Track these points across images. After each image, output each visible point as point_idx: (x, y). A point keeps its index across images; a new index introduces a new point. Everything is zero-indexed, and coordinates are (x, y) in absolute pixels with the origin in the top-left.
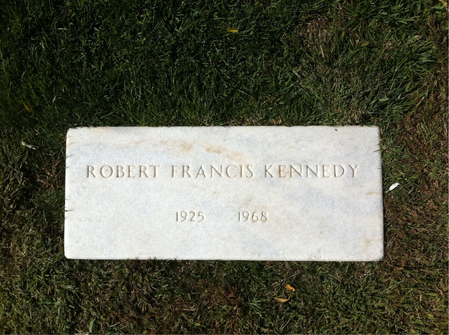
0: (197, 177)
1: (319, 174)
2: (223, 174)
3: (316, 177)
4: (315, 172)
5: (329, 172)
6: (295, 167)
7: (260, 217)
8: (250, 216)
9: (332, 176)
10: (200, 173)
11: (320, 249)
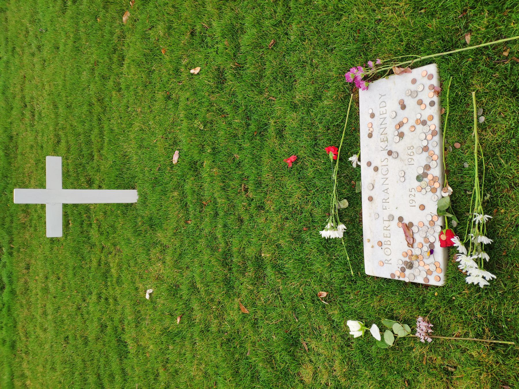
6: (381, 132)
8: (410, 157)
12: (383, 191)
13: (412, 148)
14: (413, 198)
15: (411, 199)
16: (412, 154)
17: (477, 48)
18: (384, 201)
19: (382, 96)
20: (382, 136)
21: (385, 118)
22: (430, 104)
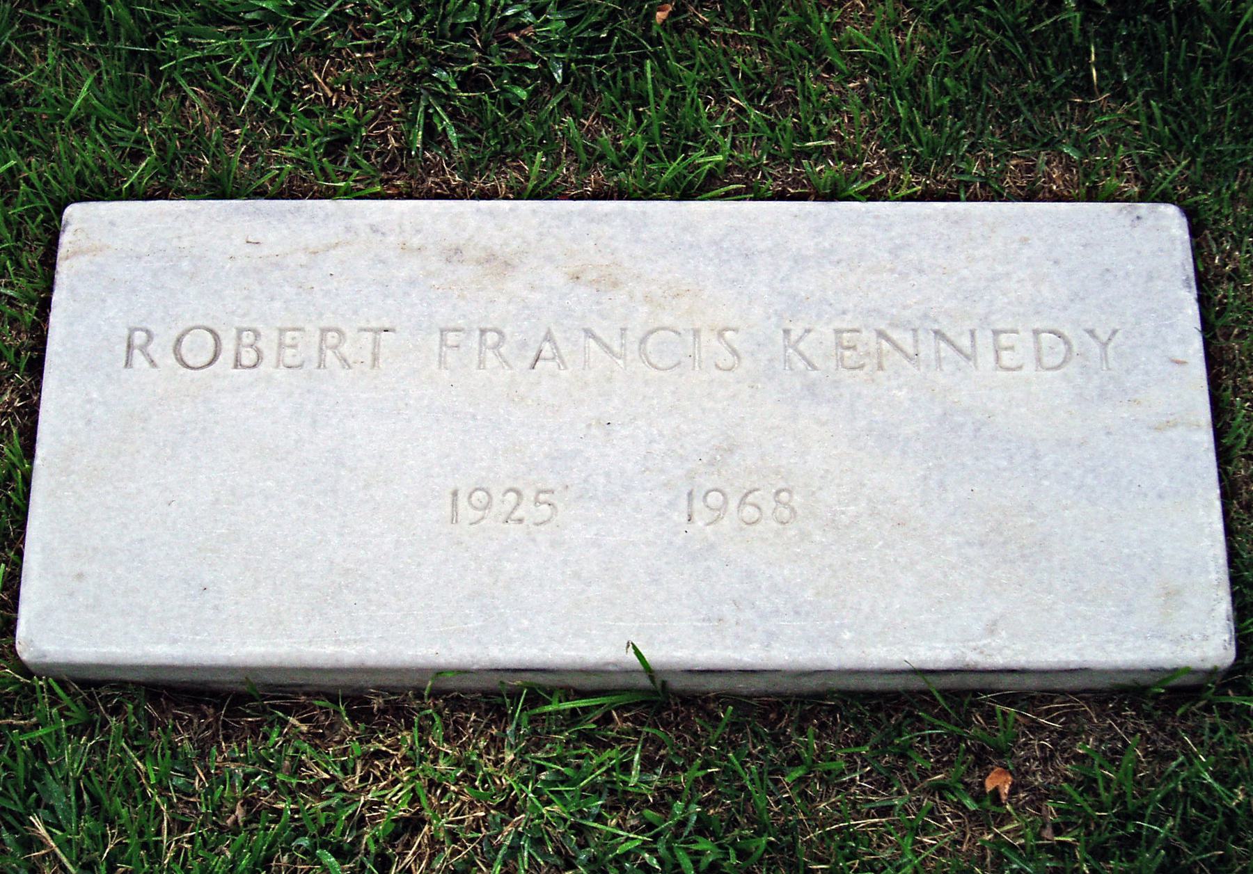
1: (986, 357)
4: (969, 351)
5: (1021, 348)
6: (895, 335)
11: (995, 623)
12: (549, 337)
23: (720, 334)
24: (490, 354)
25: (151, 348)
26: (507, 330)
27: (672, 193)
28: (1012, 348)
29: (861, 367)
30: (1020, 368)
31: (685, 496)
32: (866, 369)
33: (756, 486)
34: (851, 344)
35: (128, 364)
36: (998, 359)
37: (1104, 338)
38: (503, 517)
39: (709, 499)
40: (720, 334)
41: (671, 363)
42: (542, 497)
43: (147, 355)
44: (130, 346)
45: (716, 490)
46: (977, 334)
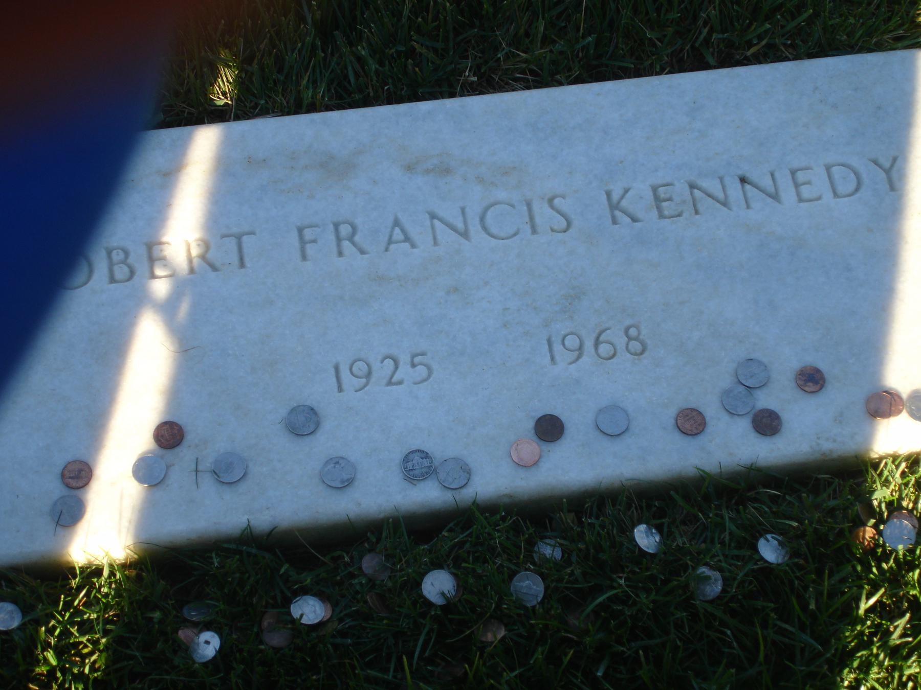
0: (387, 250)
1: (788, 194)
2: (475, 228)
3: (777, 204)
5: (818, 184)
6: (705, 183)
7: (621, 341)
8: (589, 344)
9: (828, 195)
10: (395, 237)
12: (397, 223)
13: (635, 346)
14: (383, 370)
15: (376, 366)
16: (604, 349)
17: (608, 598)
18: (345, 230)
19: (888, 172)
20: (681, 190)
21: (775, 197)
22: (337, 461)
23: (551, 201)
24: (346, 244)
25: (357, 238)
26: (358, 221)
27: (281, 111)
28: (314, 241)
29: (679, 215)
30: (819, 198)
31: (546, 342)
32: (684, 215)
33: (607, 325)
34: (668, 196)
35: (340, 254)
36: (798, 195)
37: (887, 165)
38: (385, 381)
39: (566, 342)
40: (551, 201)
41: (512, 232)
42: (417, 360)
43: (354, 244)
44: (339, 240)
45: (572, 333)
46: (777, 175)
